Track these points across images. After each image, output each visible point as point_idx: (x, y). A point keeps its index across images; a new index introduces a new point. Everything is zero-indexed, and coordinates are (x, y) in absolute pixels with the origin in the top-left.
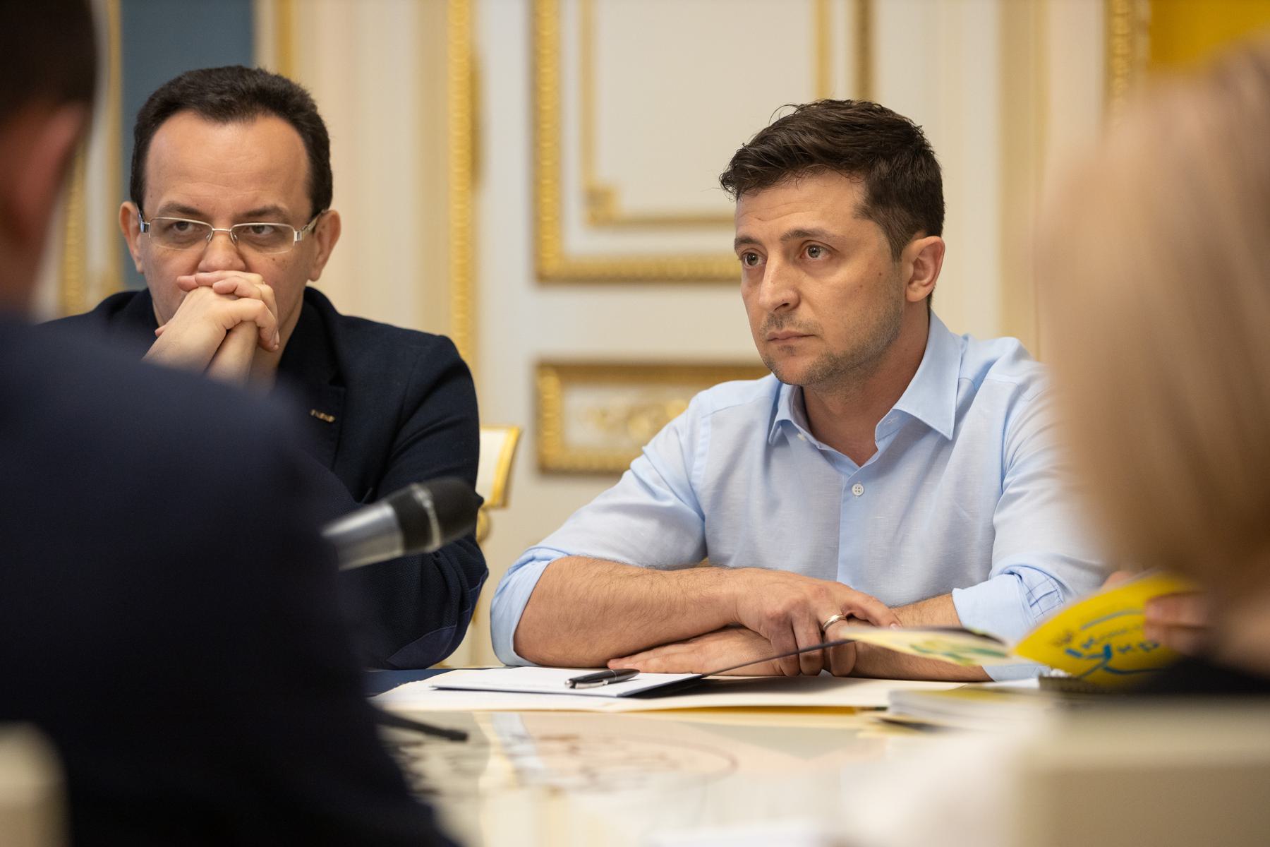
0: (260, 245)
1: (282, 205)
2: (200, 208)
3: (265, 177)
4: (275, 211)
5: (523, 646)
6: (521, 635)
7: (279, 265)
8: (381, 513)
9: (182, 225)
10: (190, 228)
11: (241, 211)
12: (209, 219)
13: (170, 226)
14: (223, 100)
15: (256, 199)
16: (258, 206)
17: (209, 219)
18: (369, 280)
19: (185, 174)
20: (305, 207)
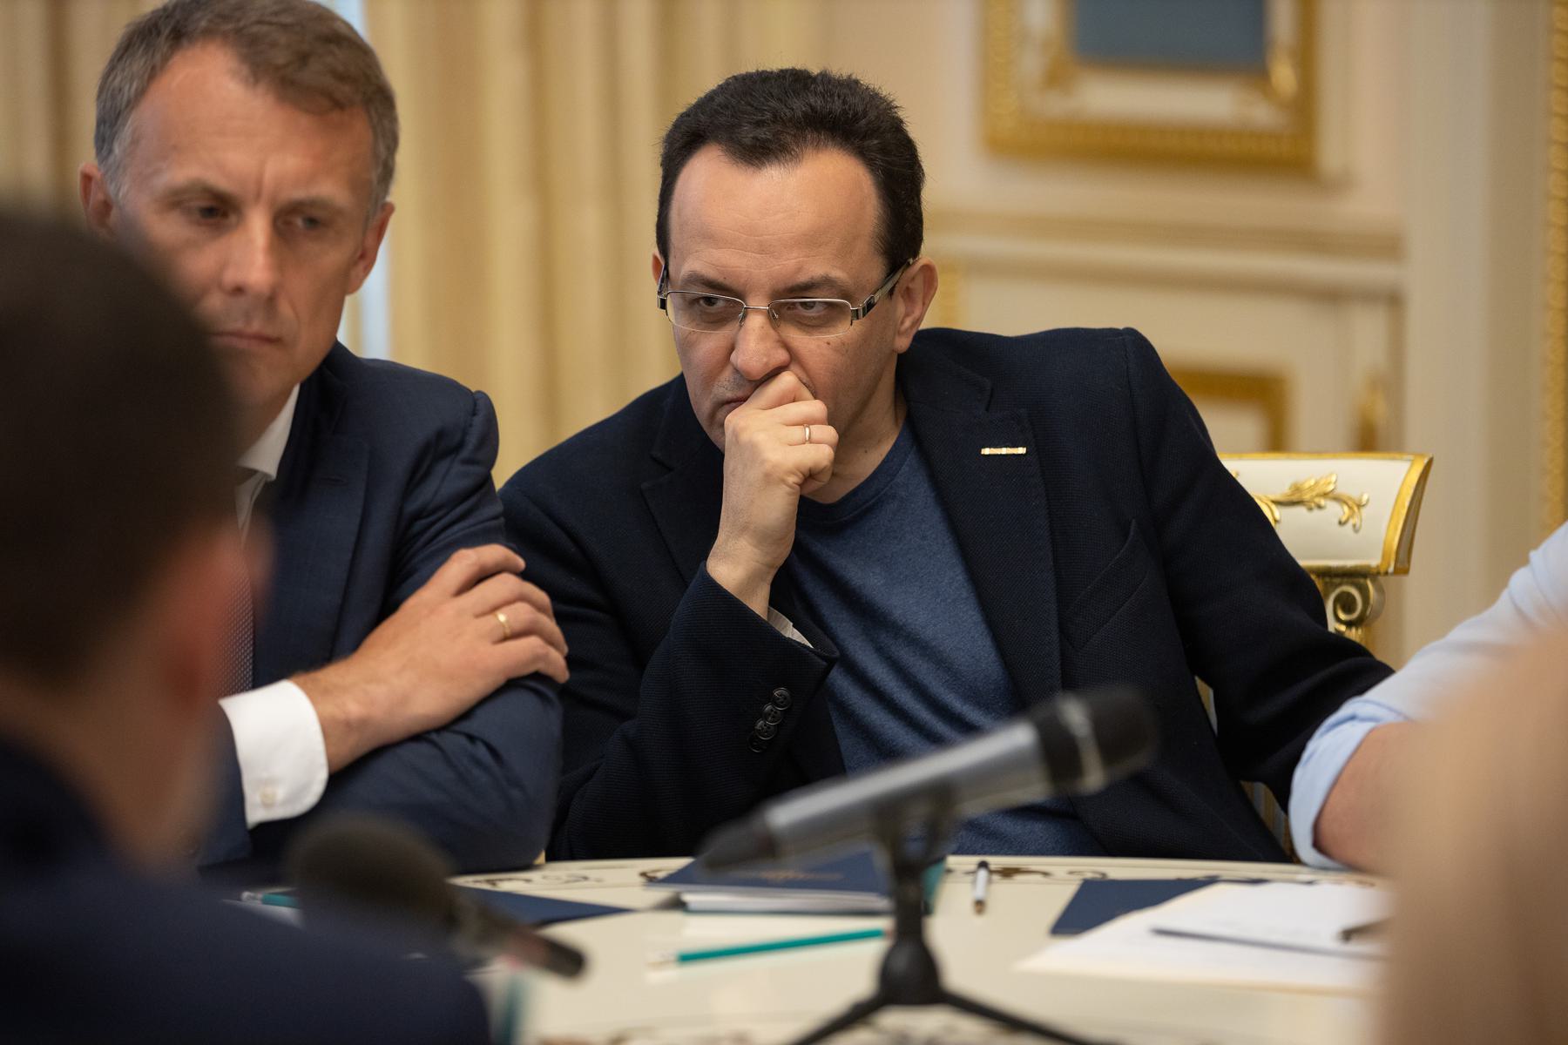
0: (809, 326)
1: (837, 274)
2: (727, 282)
3: (811, 241)
4: (826, 283)
5: (1327, 842)
6: (1325, 825)
7: (836, 350)
8: (1017, 737)
9: (710, 301)
10: (720, 304)
11: (781, 286)
12: (741, 295)
13: (696, 301)
14: (755, 138)
15: (799, 270)
16: (803, 278)
17: (741, 295)
18: (994, 290)
19: (710, 237)
20: (875, 270)
